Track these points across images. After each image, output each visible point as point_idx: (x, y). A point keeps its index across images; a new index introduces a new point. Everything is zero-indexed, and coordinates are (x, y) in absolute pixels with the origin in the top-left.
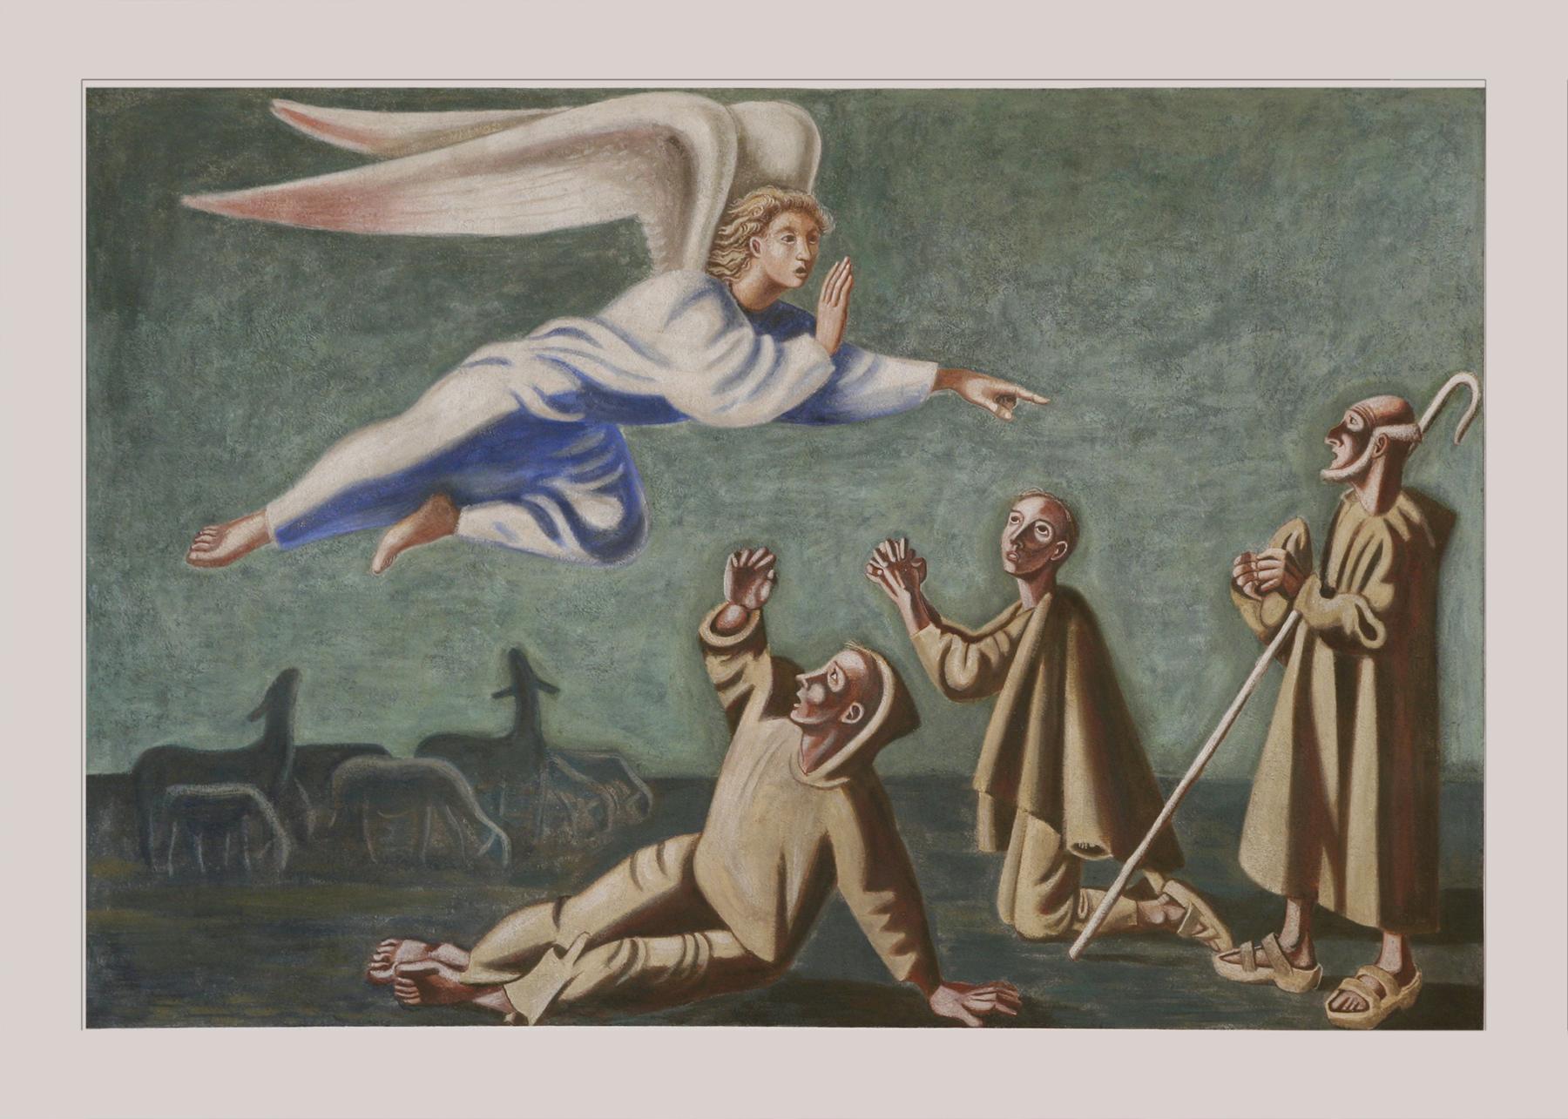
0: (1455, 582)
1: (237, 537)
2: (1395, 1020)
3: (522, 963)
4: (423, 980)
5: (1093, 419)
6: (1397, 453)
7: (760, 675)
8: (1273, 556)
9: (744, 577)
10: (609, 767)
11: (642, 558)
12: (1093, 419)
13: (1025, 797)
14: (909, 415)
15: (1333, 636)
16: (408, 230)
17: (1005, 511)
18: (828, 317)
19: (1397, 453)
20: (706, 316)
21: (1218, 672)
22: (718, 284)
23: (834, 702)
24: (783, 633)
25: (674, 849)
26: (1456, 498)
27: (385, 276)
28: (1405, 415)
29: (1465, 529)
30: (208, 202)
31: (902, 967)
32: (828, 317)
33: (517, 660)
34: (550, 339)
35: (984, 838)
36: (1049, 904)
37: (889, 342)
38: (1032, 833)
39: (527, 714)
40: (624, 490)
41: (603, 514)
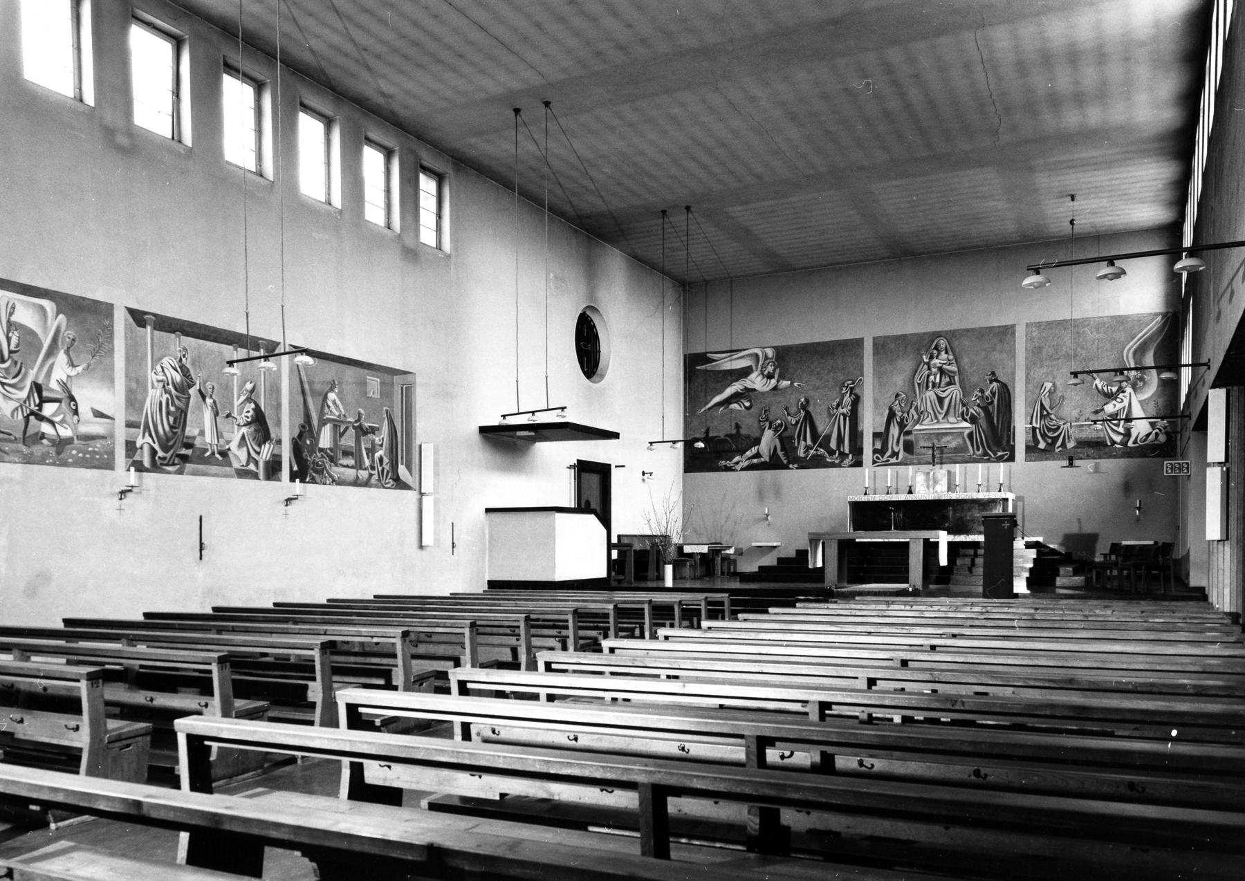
0: (860, 405)
1: (703, 410)
2: (851, 466)
3: (737, 463)
4: (725, 466)
5: (811, 387)
6: (852, 389)
7: (767, 424)
8: (835, 404)
9: (765, 411)
10: (748, 437)
11: (752, 410)
12: (811, 387)
13: (801, 438)
14: (786, 388)
15: (843, 414)
16: (725, 369)
17: (799, 400)
18: (776, 376)
19: (852, 389)
20: (760, 378)
21: (827, 420)
22: (762, 373)
23: (777, 427)
24: (771, 418)
25: (756, 447)
26: (860, 394)
27: (720, 375)
28: (853, 384)
29: (861, 401)
30: (699, 368)
31: (785, 462)
32: (776, 376)
33: (737, 424)
34: (741, 382)
35: (796, 445)
36: (805, 453)
37: (784, 379)
38: (803, 443)
39: (738, 432)
40: (750, 401)
41: (747, 404)
